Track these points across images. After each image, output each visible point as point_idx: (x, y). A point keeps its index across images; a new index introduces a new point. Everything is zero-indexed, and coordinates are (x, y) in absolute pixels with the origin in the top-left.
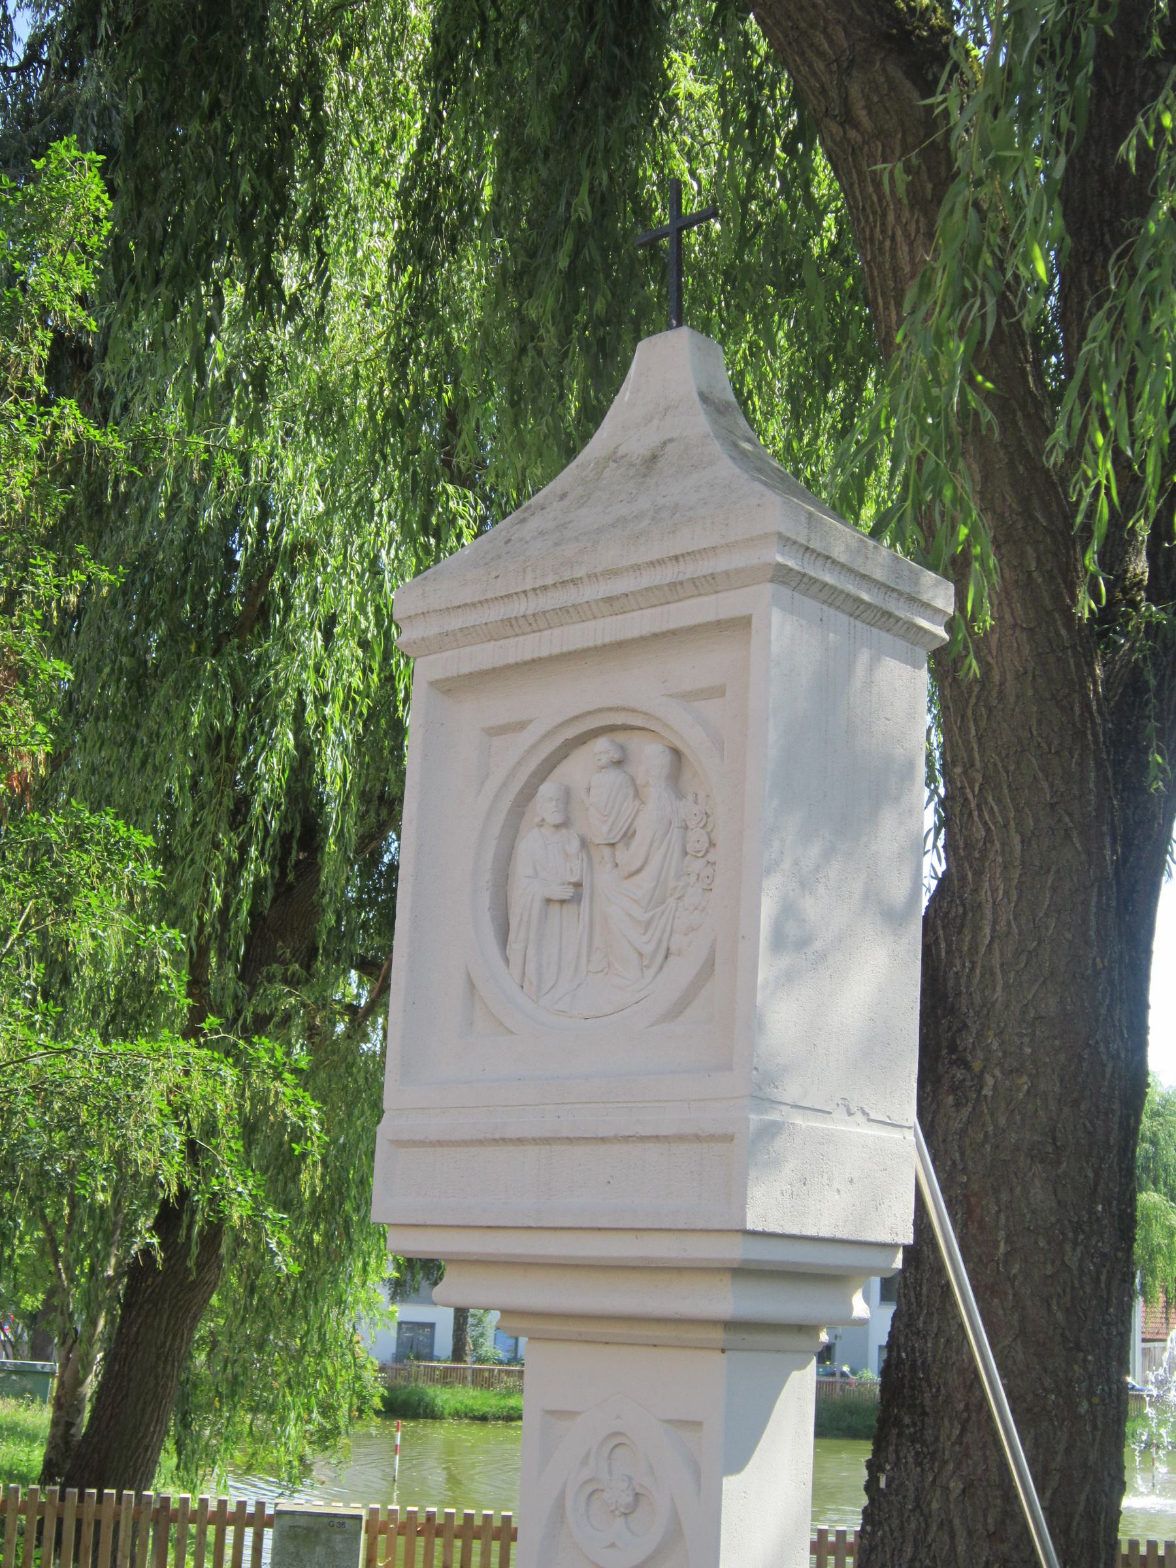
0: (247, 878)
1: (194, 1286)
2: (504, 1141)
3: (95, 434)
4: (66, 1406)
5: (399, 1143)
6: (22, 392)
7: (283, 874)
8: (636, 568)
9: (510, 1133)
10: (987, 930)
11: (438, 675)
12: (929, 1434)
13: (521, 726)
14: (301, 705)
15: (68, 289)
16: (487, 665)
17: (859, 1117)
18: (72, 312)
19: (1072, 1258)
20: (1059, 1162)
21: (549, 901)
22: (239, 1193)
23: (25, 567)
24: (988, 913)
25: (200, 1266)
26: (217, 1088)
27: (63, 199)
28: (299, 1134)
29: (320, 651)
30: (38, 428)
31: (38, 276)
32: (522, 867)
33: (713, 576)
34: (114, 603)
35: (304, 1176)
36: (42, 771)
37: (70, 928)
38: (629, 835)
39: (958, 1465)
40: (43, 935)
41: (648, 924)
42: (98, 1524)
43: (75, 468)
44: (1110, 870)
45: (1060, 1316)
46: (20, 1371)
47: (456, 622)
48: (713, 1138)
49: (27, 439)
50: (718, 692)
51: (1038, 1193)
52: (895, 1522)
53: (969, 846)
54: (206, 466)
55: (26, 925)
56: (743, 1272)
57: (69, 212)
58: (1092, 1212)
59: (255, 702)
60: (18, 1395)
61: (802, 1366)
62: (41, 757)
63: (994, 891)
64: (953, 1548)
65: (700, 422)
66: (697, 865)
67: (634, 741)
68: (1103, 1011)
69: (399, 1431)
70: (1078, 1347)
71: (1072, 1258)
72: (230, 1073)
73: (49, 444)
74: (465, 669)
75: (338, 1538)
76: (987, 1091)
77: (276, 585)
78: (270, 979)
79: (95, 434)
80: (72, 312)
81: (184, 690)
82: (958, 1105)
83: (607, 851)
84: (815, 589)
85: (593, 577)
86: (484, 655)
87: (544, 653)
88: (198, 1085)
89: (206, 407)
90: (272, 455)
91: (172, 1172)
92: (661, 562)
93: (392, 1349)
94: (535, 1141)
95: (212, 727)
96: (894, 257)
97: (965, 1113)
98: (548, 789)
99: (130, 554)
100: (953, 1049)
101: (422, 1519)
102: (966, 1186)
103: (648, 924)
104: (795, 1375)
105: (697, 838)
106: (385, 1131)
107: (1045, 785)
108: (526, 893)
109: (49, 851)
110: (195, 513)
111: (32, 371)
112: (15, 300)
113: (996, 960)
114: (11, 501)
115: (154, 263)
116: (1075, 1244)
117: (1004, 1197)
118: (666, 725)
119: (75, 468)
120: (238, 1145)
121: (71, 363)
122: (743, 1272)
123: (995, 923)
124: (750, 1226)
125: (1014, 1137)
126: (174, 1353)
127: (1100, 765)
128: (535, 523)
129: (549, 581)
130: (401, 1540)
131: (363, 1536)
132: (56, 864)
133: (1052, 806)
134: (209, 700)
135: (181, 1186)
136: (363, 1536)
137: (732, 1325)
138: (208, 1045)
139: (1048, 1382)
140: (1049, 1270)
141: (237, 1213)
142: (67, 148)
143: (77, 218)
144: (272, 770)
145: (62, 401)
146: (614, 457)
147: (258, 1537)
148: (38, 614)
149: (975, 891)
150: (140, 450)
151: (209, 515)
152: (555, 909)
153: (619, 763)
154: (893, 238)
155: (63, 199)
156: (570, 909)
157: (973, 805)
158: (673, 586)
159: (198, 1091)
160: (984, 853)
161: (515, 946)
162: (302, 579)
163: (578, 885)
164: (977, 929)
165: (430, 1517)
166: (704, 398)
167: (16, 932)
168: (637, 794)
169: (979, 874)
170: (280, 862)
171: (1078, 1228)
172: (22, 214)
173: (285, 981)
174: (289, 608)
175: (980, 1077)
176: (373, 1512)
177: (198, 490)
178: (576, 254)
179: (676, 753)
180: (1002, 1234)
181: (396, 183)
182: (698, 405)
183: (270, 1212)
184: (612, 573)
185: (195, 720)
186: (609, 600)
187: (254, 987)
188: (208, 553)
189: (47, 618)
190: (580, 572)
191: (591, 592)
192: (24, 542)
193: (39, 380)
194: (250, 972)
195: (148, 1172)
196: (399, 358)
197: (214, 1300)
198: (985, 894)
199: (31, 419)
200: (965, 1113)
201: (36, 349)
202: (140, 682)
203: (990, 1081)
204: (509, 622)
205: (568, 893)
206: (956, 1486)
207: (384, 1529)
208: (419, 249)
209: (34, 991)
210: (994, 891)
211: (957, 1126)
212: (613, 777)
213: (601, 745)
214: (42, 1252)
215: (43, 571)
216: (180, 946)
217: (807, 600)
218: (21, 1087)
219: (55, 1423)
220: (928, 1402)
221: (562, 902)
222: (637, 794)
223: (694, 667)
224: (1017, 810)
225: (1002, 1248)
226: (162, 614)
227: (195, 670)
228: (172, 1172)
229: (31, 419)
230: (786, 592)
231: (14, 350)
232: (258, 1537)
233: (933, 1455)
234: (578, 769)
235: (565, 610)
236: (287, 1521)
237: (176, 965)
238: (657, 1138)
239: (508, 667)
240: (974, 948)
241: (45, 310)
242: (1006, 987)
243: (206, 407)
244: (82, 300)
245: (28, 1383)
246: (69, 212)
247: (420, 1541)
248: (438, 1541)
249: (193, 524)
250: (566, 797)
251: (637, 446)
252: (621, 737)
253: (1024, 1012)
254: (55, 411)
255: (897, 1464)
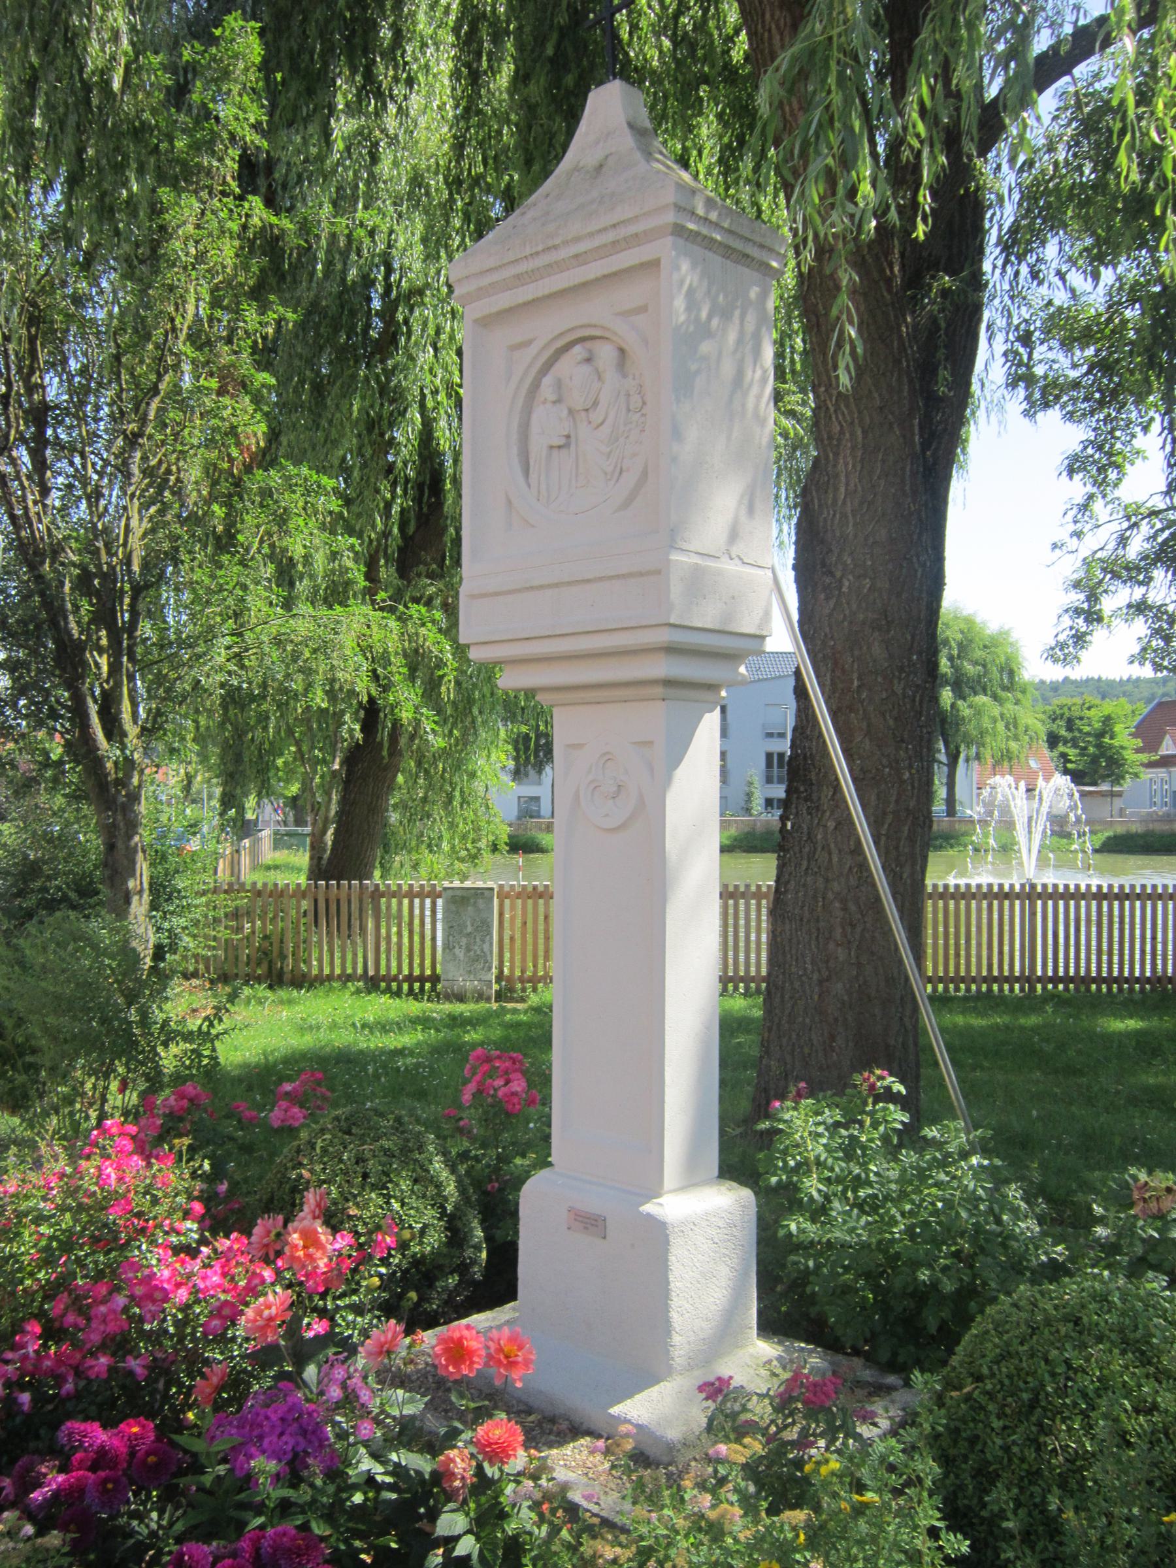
0: (396, 509)
1: (386, 769)
2: (532, 588)
3: (274, 220)
4: (316, 848)
5: (473, 597)
6: (224, 194)
7: (421, 509)
8: (591, 235)
9: (536, 583)
10: (842, 489)
11: (478, 315)
12: (815, 796)
13: (527, 343)
14: (423, 396)
15: (247, 119)
16: (507, 305)
17: (737, 561)
18: (251, 137)
19: (898, 688)
20: (889, 631)
21: (551, 447)
22: (406, 702)
23: (237, 312)
24: (843, 479)
25: (391, 755)
26: (388, 634)
27: (236, 56)
28: (440, 664)
29: (432, 359)
30: (235, 216)
31: (225, 111)
32: (535, 429)
33: (636, 235)
34: (297, 336)
35: (443, 689)
36: (262, 444)
37: (287, 542)
38: (596, 404)
39: (832, 813)
40: (272, 546)
41: (609, 455)
42: (338, 901)
43: (267, 244)
44: (918, 448)
45: (891, 722)
46: (288, 834)
47: (486, 281)
48: (648, 573)
49: (230, 224)
50: (643, 309)
51: (877, 650)
52: (797, 849)
53: (830, 438)
54: (349, 237)
55: (262, 541)
56: (671, 650)
57: (241, 65)
58: (910, 660)
59: (392, 397)
60: (289, 847)
61: (711, 711)
62: (260, 435)
63: (846, 464)
64: (830, 860)
65: (628, 141)
66: (635, 417)
67: (597, 346)
68: (915, 537)
69: (520, 859)
70: (902, 741)
71: (898, 688)
72: (393, 624)
73: (245, 227)
74: (494, 310)
75: (480, 901)
76: (844, 589)
77: (401, 318)
78: (419, 575)
79: (274, 220)
80: (251, 137)
81: (347, 392)
82: (827, 599)
83: (583, 414)
84: (699, 239)
85: (566, 243)
86: (504, 300)
87: (540, 294)
88: (377, 634)
89: (343, 202)
90: (391, 232)
91: (363, 686)
92: (605, 229)
93: (515, 813)
94: (550, 586)
95: (368, 414)
96: (771, 45)
97: (832, 603)
98: (547, 381)
99: (305, 303)
100: (823, 565)
101: (530, 889)
102: (833, 647)
103: (609, 455)
104: (707, 715)
105: (636, 400)
106: (463, 591)
107: (876, 395)
108: (538, 444)
109: (271, 495)
110: (344, 272)
111: (229, 179)
112: (212, 130)
113: (849, 509)
114: (224, 267)
115: (296, 90)
116: (900, 679)
117: (856, 653)
118: (615, 334)
119: (267, 244)
120: (405, 670)
121: (255, 173)
122: (671, 650)
123: (847, 484)
124: (672, 621)
125: (861, 617)
126: (376, 810)
127: (911, 381)
128: (531, 214)
129: (540, 248)
130: (519, 901)
131: (496, 901)
132: (276, 502)
133: (881, 408)
134: (363, 398)
135: (369, 695)
136: (496, 901)
137: (668, 683)
138: (382, 609)
139: (884, 761)
140: (884, 695)
141: (406, 715)
142: (235, 19)
143: (247, 69)
144: (406, 435)
145: (250, 197)
146: (577, 169)
147: (434, 904)
148: (249, 342)
149: (835, 466)
150: (305, 228)
151: (353, 273)
152: (555, 452)
153: (588, 360)
154: (770, 31)
155: (236, 56)
156: (564, 451)
157: (832, 409)
158: (614, 243)
159: (376, 637)
160: (839, 440)
161: (533, 476)
162: (417, 313)
163: (568, 437)
164: (836, 489)
165: (535, 888)
166: (631, 126)
167: (256, 546)
168: (600, 378)
169: (836, 455)
170: (418, 500)
171: (901, 669)
172: (210, 67)
173: (428, 577)
174: (409, 334)
175: (840, 581)
176: (501, 886)
177: (345, 255)
178: (558, 47)
179: (622, 351)
180: (855, 675)
181: (451, 24)
182: (627, 130)
183: (424, 710)
184: (577, 239)
185: (355, 408)
186: (576, 256)
187: (409, 582)
188: (356, 300)
189: (255, 342)
190: (557, 241)
191: (564, 253)
192: (236, 296)
193: (234, 185)
194: (404, 570)
195: (347, 687)
196: (459, 146)
197: (400, 778)
198: (841, 466)
199: (231, 211)
200: (832, 603)
201: (228, 162)
202: (319, 389)
203: (846, 583)
204: (518, 277)
205: (562, 441)
206: (831, 824)
207: (507, 896)
208: (471, 74)
209: (269, 581)
210: (846, 464)
211: (827, 611)
212: (586, 369)
213: (577, 349)
214: (295, 759)
215: (251, 315)
216: (358, 548)
217: (696, 248)
218: (266, 639)
219: (311, 858)
220: (814, 777)
221: (559, 447)
222: (600, 378)
223: (630, 295)
224: (860, 412)
225: (856, 683)
226: (328, 340)
227: (354, 377)
228: (363, 686)
229: (231, 211)
230: (681, 242)
231: (215, 164)
232: (434, 904)
233: (818, 808)
234: (567, 366)
235: (550, 265)
236: (450, 893)
237: (356, 561)
238: (618, 577)
239: (519, 306)
240: (835, 500)
241: (232, 137)
242: (855, 524)
243: (343, 202)
244: (256, 127)
245: (294, 841)
246: (241, 65)
247: (530, 902)
248: (541, 901)
249: (344, 280)
250: (559, 385)
251: (591, 159)
252: (588, 344)
253: (866, 539)
254: (246, 205)
255: (797, 814)
